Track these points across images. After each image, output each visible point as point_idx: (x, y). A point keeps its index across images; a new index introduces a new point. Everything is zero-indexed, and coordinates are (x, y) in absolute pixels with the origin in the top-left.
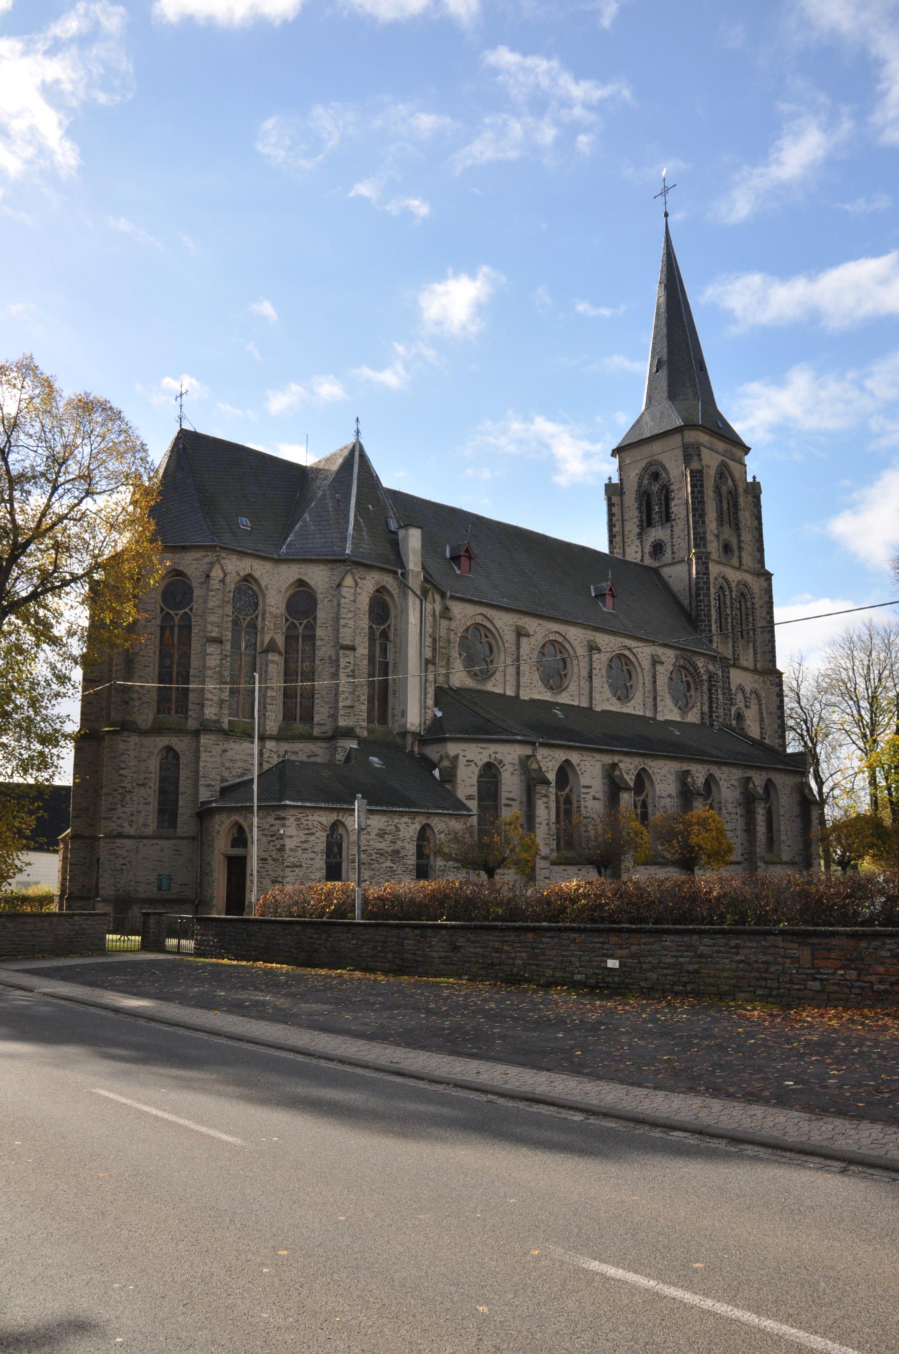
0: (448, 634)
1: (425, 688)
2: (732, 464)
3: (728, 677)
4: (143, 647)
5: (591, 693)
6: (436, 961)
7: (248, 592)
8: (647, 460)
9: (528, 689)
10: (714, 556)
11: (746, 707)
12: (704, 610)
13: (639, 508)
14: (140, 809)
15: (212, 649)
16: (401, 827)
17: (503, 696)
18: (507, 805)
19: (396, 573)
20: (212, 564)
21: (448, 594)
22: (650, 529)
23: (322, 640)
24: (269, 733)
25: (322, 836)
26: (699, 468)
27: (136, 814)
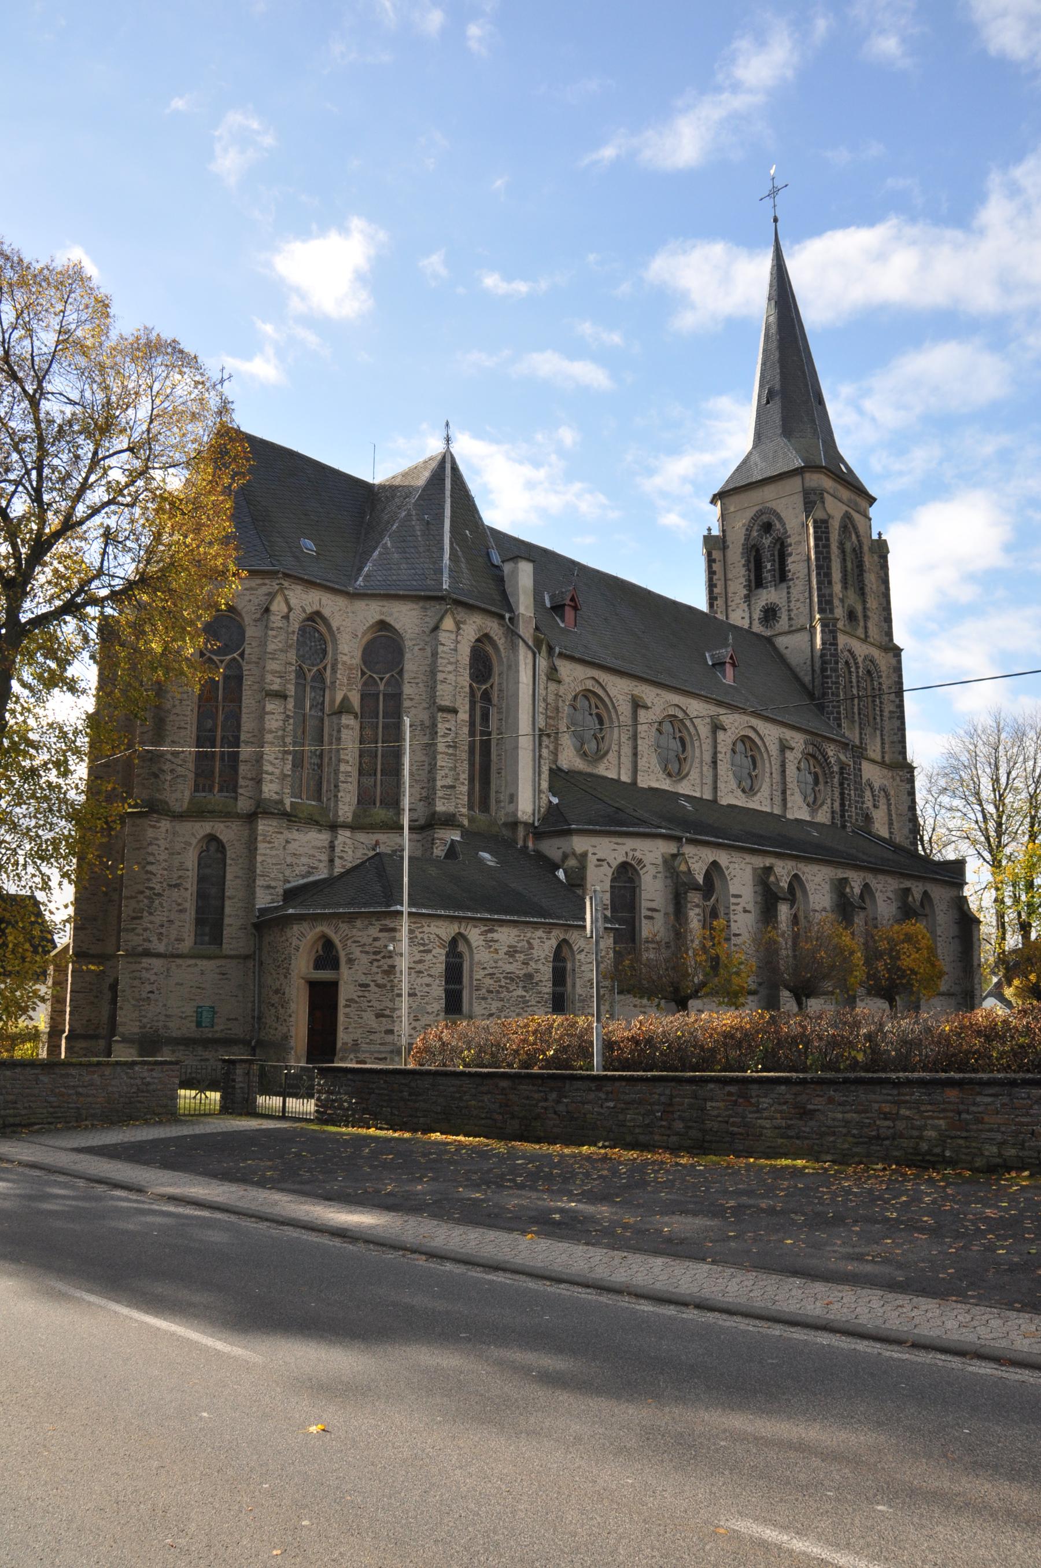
0: (556, 700)
1: (539, 767)
2: (856, 516)
3: (860, 770)
4: (177, 702)
5: (715, 782)
6: (768, 1133)
7: (315, 632)
8: (757, 508)
9: (646, 774)
10: (840, 625)
11: (875, 806)
12: (831, 688)
13: (747, 565)
14: (172, 918)
15: (273, 706)
16: (535, 943)
17: (618, 781)
18: (648, 917)
19: (502, 617)
20: (272, 596)
21: (557, 650)
22: (760, 591)
23: (411, 699)
24: (341, 819)
25: (440, 954)
26: (825, 517)
27: (166, 924)
